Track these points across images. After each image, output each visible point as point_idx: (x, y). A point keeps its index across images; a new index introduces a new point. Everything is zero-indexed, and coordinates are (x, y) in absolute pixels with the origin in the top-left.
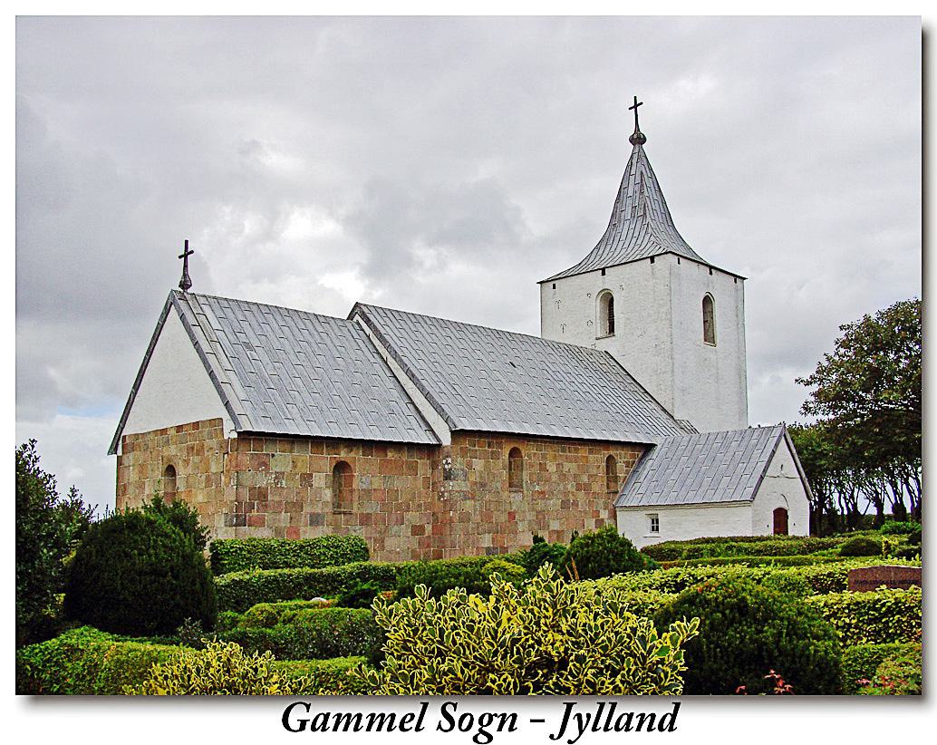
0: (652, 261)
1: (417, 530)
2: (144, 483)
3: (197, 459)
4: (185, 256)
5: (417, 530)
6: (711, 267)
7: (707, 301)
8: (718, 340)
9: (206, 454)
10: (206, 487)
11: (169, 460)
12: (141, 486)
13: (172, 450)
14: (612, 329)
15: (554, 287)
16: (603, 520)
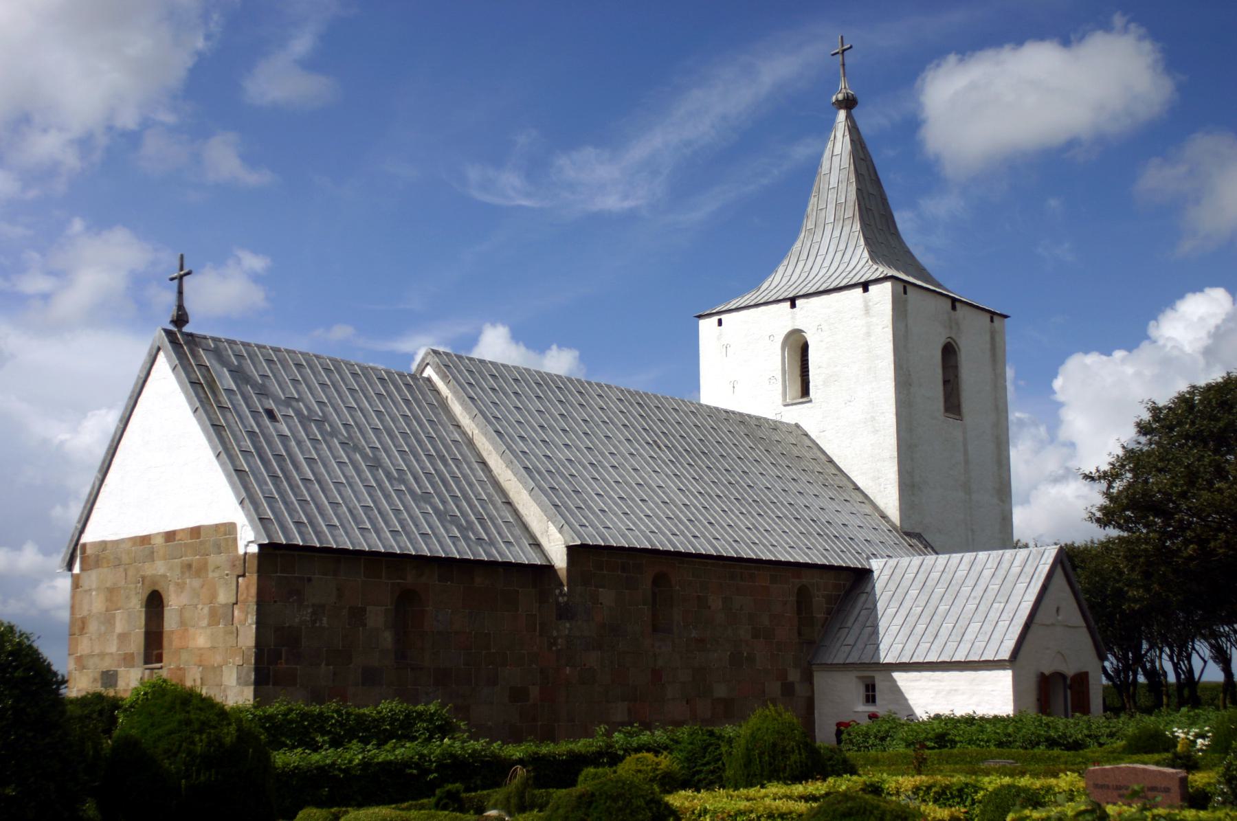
0: (793, 306)
1: (518, 695)
2: (114, 617)
3: (196, 583)
4: (181, 277)
5: (518, 695)
6: (954, 300)
7: (949, 352)
8: (966, 407)
9: (211, 575)
10: (209, 625)
12: (109, 620)
13: (159, 568)
14: (805, 391)
15: (720, 323)
16: (792, 684)
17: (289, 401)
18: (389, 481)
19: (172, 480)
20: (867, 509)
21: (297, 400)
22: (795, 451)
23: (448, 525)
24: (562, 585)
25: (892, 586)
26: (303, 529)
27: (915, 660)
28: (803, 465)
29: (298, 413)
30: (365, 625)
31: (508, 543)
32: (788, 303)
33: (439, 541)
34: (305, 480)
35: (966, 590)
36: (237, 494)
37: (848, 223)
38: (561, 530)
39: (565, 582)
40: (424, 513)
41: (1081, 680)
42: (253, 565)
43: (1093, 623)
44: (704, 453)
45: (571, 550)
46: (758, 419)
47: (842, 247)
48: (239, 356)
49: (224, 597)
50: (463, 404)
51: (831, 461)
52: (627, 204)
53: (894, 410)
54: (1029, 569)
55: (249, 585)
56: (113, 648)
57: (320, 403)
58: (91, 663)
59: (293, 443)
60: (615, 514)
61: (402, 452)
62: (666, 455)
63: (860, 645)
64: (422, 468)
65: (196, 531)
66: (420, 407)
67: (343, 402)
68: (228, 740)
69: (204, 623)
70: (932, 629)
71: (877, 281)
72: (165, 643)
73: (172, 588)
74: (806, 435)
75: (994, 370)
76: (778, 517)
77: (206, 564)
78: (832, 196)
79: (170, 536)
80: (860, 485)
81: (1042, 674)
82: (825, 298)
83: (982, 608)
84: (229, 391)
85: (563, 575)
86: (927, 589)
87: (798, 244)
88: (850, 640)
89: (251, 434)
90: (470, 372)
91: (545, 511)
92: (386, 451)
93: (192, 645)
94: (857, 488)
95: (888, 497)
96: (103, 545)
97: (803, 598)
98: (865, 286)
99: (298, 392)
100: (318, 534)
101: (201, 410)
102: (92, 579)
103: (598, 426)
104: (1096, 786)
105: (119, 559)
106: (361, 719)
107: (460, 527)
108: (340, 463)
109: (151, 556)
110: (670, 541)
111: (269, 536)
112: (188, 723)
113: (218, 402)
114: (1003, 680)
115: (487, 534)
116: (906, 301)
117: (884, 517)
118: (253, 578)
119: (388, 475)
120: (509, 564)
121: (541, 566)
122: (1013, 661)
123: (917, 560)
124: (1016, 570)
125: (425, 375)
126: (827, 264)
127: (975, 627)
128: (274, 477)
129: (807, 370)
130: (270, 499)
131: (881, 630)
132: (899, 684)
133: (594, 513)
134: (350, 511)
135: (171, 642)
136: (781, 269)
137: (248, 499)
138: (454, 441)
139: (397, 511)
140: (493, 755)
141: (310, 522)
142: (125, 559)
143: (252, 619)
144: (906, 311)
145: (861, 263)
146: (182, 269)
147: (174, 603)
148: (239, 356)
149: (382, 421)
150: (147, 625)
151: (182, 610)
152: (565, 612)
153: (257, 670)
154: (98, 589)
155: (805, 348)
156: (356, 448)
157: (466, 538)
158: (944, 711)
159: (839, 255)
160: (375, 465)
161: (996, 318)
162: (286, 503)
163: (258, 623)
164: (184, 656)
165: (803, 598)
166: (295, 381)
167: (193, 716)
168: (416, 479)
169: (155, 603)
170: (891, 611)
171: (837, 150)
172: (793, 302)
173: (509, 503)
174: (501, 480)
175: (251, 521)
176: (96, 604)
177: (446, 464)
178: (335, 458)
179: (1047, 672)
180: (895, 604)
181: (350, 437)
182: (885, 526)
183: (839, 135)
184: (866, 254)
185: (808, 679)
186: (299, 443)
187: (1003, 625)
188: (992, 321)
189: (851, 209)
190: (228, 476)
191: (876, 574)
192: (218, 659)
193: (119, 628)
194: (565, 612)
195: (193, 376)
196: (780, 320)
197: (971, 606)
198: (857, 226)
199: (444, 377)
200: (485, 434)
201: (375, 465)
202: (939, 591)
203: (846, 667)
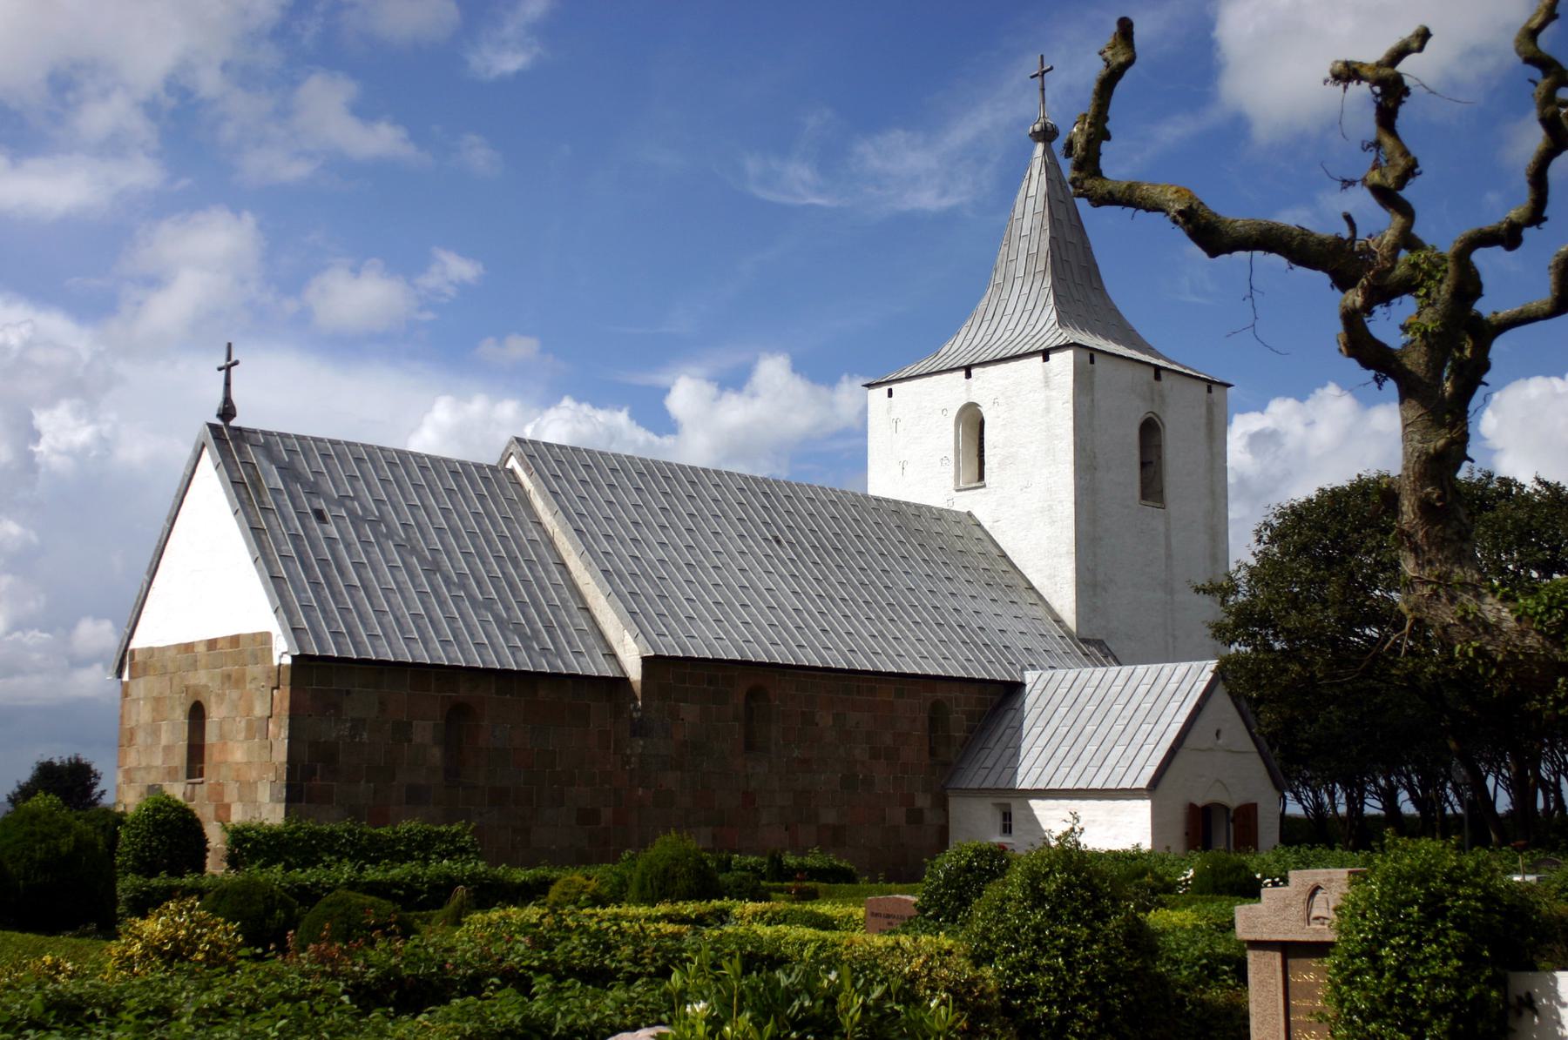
1: (588, 817)
3: (235, 694)
4: (228, 369)
5: (588, 817)
7: (1150, 430)
10: (246, 738)
11: (197, 693)
12: (155, 732)
13: (201, 678)
14: (981, 477)
15: (890, 393)
16: (921, 811)
17: (342, 500)
18: (447, 586)
19: (213, 589)
20: (1040, 612)
21: (352, 499)
22: (959, 546)
23: (509, 634)
24: (636, 699)
25: (1042, 702)
26: (341, 639)
27: (1051, 786)
28: (966, 560)
29: (351, 513)
30: (410, 741)
31: (578, 653)
32: (963, 373)
33: (496, 652)
34: (350, 587)
35: (1117, 707)
36: (272, 602)
37: (1039, 277)
38: (636, 638)
39: (639, 694)
40: (483, 622)
41: (1247, 813)
42: (286, 677)
43: (1266, 748)
44: (836, 549)
45: (645, 660)
46: (918, 507)
47: (1030, 306)
48: (291, 452)
49: (260, 710)
50: (544, 499)
51: (1004, 556)
52: (946, 202)
53: (1072, 498)
54: (1186, 687)
55: (283, 697)
56: (158, 761)
57: (378, 501)
58: (138, 776)
59: (341, 546)
60: (705, 622)
61: (466, 554)
62: (786, 553)
63: (998, 768)
64: (488, 572)
65: (235, 640)
66: (495, 503)
67: (405, 499)
68: (64, 849)
69: (242, 736)
70: (1074, 753)
71: (1058, 348)
72: (207, 758)
73: (213, 699)
74: (979, 525)
75: (1211, 448)
76: (916, 623)
77: (244, 675)
78: (1024, 245)
79: (212, 644)
80: (1035, 584)
81: (1192, 807)
82: (1013, 365)
83: (1130, 730)
84: (275, 491)
85: (637, 688)
86: (1078, 707)
87: (985, 301)
88: (989, 763)
89: (295, 537)
90: (558, 462)
91: (621, 618)
92: (448, 553)
93: (230, 759)
94: (1031, 588)
95: (1063, 598)
96: (151, 651)
97: (937, 717)
98: (1045, 354)
99: (354, 489)
100: (356, 645)
101: (241, 512)
102: (140, 688)
103: (706, 520)
104: (873, 914)
105: (164, 667)
106: (374, 840)
107: (523, 637)
108: (392, 568)
109: (194, 665)
110: (766, 651)
111: (300, 648)
112: (32, 834)
113: (261, 502)
114: (1143, 808)
115: (554, 643)
116: (1093, 371)
117: (1058, 621)
118: (286, 690)
119: (447, 580)
120: (576, 676)
121: (614, 679)
122: (1154, 787)
123: (1100, 671)
124: (1172, 686)
125: (509, 466)
126: (1011, 326)
127: (1119, 750)
128: (315, 584)
129: (987, 450)
130: (307, 608)
131: (1023, 752)
132: (1036, 813)
133: (678, 620)
134: (397, 619)
135: (212, 755)
136: (964, 331)
137: (284, 607)
138: (532, 541)
139: (451, 619)
140: (496, 878)
141: (350, 633)
142: (171, 667)
143: (285, 733)
144: (1092, 383)
145: (1045, 324)
146: (229, 358)
147: (215, 714)
148: (291, 452)
149: (447, 520)
150: (190, 738)
151: (221, 723)
152: (640, 729)
153: (289, 787)
154: (145, 698)
155: (982, 423)
156: (414, 551)
157: (528, 649)
158: (1113, 848)
159: (1026, 315)
160: (433, 568)
161: (1214, 387)
162: (324, 611)
163: (291, 738)
164: (224, 770)
165: (937, 717)
166: (352, 478)
167: (37, 829)
168: (479, 584)
169: (197, 714)
170: (1036, 730)
171: (1032, 192)
172: (968, 370)
173: (586, 609)
174: (580, 583)
175: (284, 631)
176: (142, 714)
177: (516, 566)
178: (387, 562)
179: (1200, 803)
180: (1041, 723)
181: (409, 539)
182: (1056, 631)
183: (1035, 173)
184: (1054, 316)
185: (942, 804)
186: (348, 546)
187: (1148, 748)
188: (1209, 390)
189: (1043, 262)
190: (265, 583)
191: (1028, 689)
192: (254, 774)
193: (165, 739)
194: (640, 729)
195: (236, 475)
196: (951, 392)
197: (1119, 728)
198: (1048, 282)
199: (527, 469)
200: (565, 533)
201: (433, 568)
202: (1090, 708)
203: (981, 792)
